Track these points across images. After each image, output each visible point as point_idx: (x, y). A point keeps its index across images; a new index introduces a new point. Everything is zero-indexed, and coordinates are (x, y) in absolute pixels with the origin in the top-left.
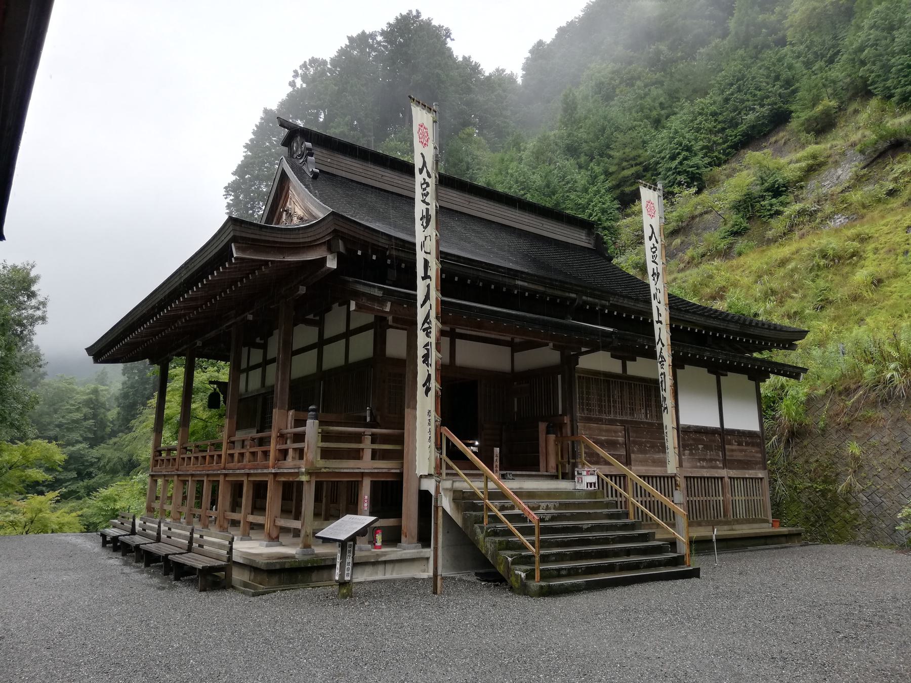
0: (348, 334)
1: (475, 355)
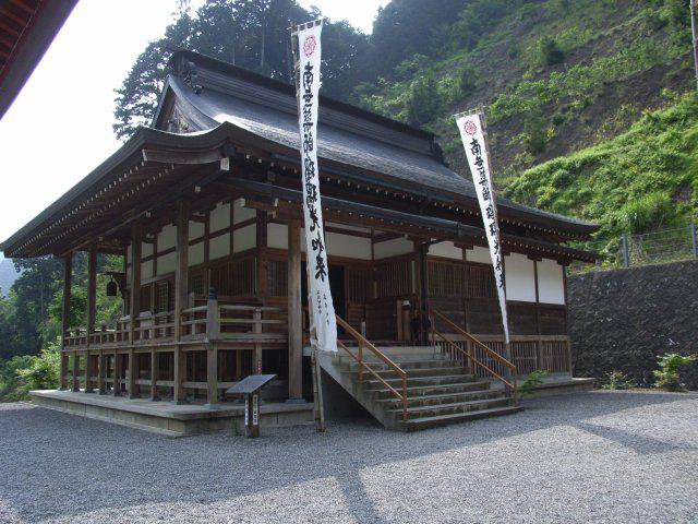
0: (232, 228)
1: (357, 249)
